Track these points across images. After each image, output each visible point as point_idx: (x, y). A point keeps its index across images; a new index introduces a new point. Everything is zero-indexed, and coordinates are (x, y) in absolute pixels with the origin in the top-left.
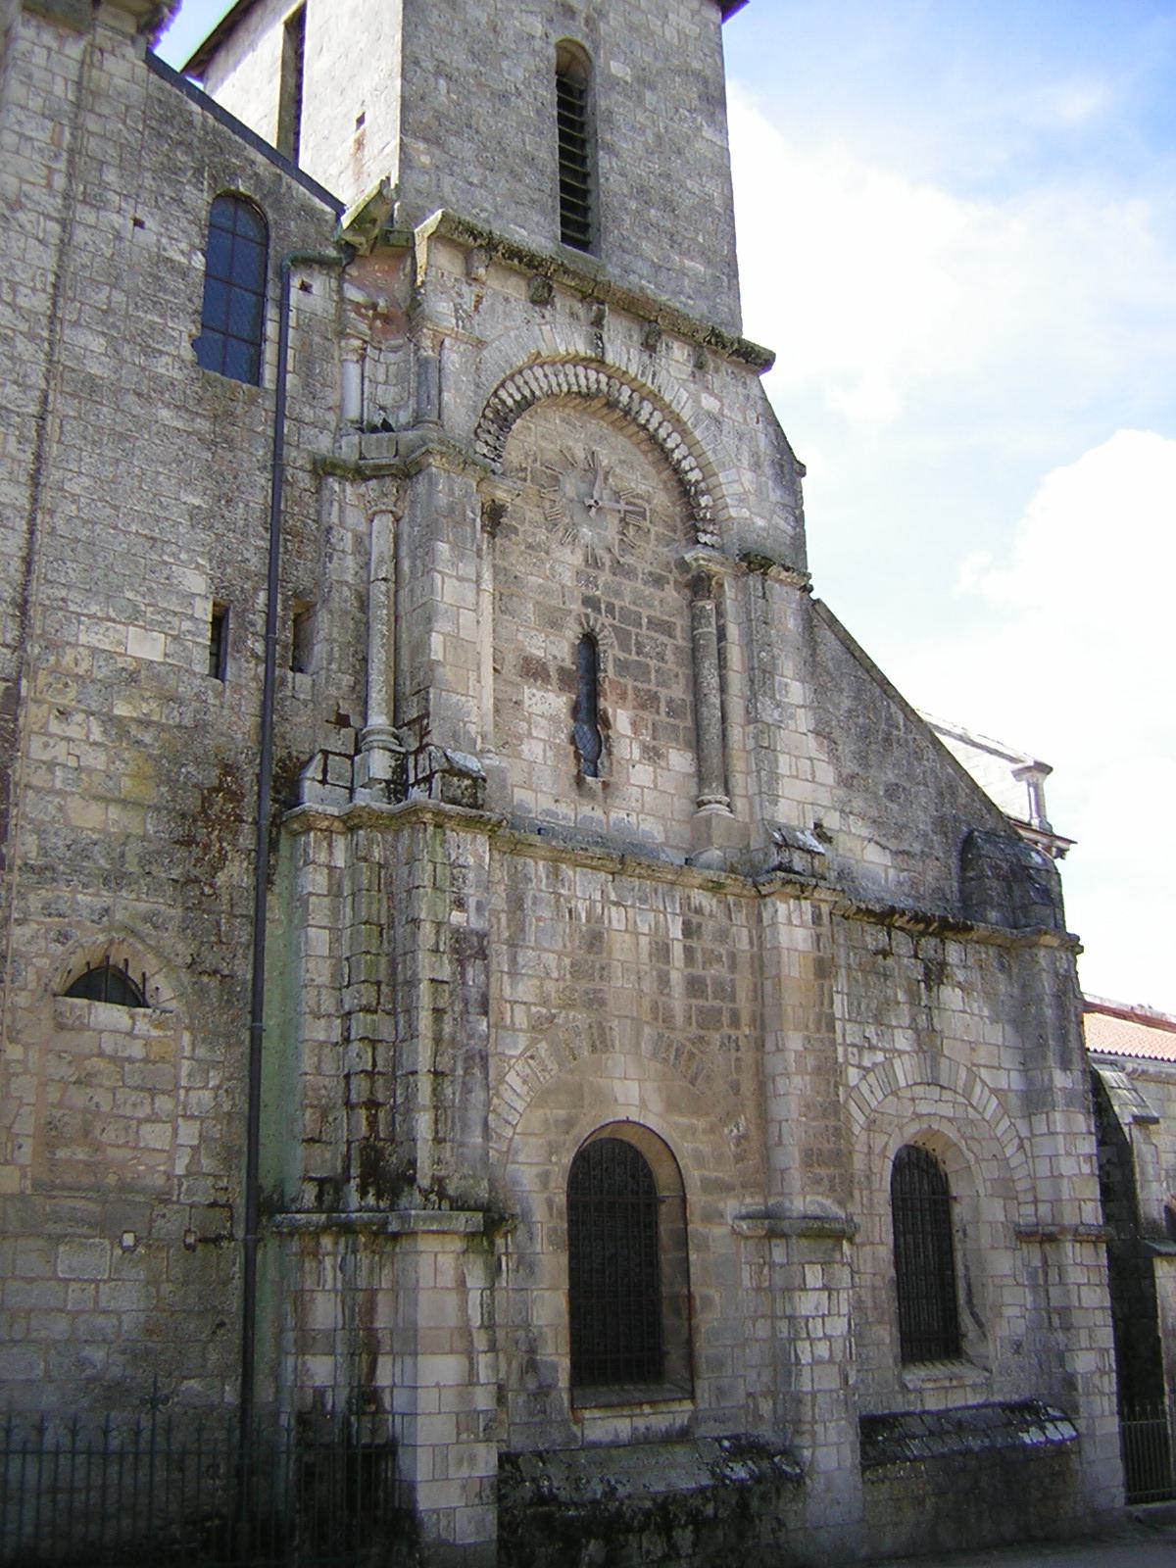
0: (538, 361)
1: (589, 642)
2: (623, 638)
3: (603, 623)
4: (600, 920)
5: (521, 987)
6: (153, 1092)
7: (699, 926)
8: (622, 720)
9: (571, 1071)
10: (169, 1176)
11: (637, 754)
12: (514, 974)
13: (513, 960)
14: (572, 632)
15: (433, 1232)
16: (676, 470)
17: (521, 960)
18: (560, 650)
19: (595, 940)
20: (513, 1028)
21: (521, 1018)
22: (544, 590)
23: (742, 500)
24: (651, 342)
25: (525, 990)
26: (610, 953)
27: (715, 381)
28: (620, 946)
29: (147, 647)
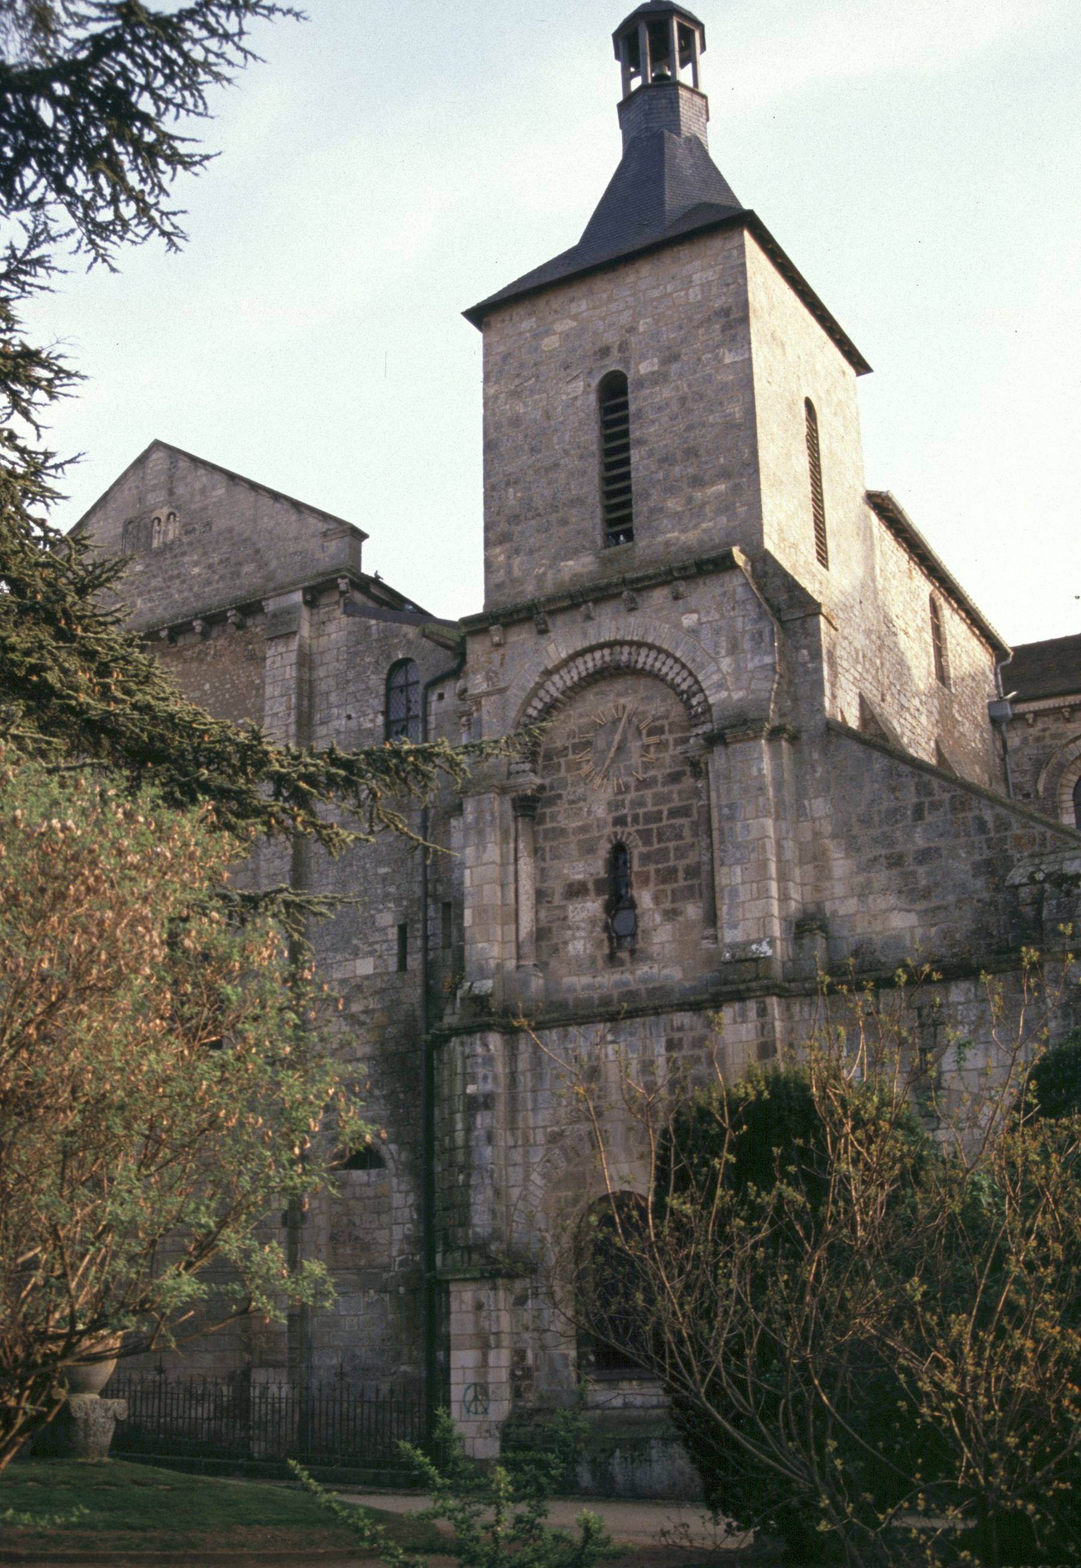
0: (548, 673)
1: (619, 850)
2: (645, 836)
3: (629, 834)
4: (598, 1058)
5: (540, 1117)
6: (379, 1213)
7: (681, 1040)
8: (645, 898)
9: (577, 1165)
10: (390, 1256)
11: (658, 918)
12: (535, 1110)
13: (535, 1100)
14: (604, 849)
15: (460, 1280)
16: (674, 687)
17: (540, 1099)
18: (596, 867)
19: (594, 1073)
20: (535, 1145)
21: (540, 1138)
22: (583, 829)
23: (721, 686)
24: (693, 570)
25: (543, 1118)
26: (606, 1080)
27: (693, 600)
28: (612, 1072)
29: (365, 967)
